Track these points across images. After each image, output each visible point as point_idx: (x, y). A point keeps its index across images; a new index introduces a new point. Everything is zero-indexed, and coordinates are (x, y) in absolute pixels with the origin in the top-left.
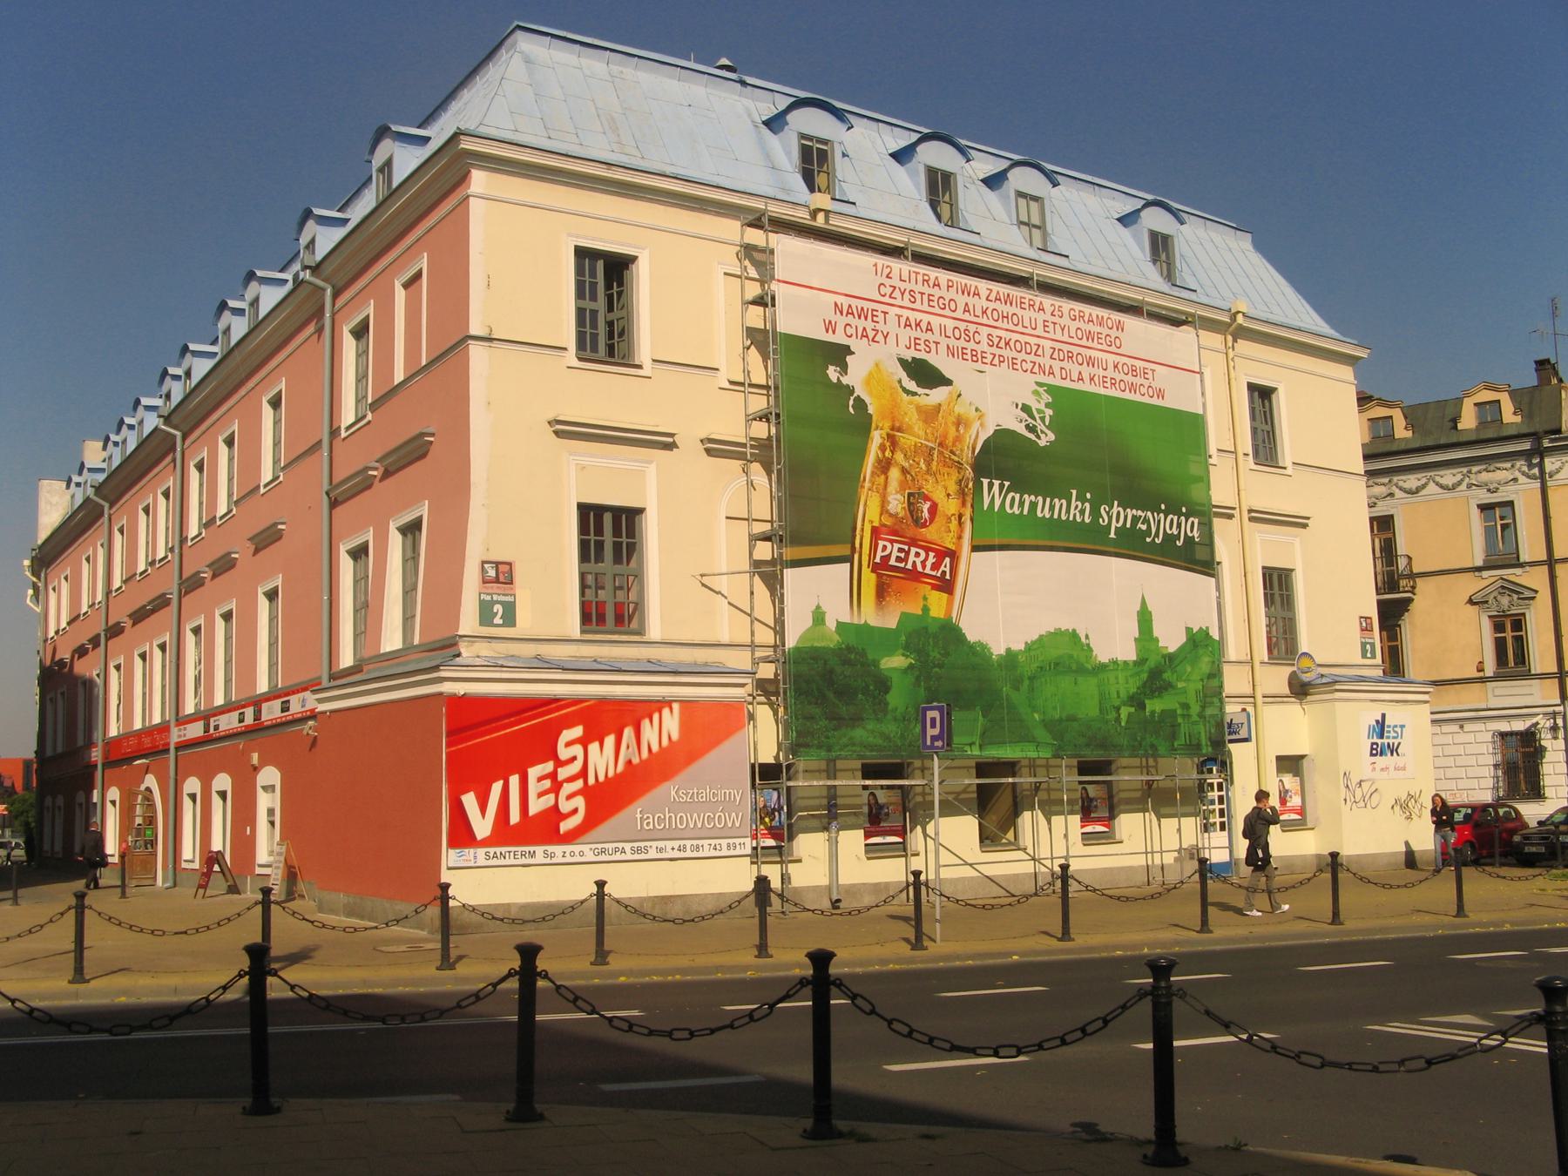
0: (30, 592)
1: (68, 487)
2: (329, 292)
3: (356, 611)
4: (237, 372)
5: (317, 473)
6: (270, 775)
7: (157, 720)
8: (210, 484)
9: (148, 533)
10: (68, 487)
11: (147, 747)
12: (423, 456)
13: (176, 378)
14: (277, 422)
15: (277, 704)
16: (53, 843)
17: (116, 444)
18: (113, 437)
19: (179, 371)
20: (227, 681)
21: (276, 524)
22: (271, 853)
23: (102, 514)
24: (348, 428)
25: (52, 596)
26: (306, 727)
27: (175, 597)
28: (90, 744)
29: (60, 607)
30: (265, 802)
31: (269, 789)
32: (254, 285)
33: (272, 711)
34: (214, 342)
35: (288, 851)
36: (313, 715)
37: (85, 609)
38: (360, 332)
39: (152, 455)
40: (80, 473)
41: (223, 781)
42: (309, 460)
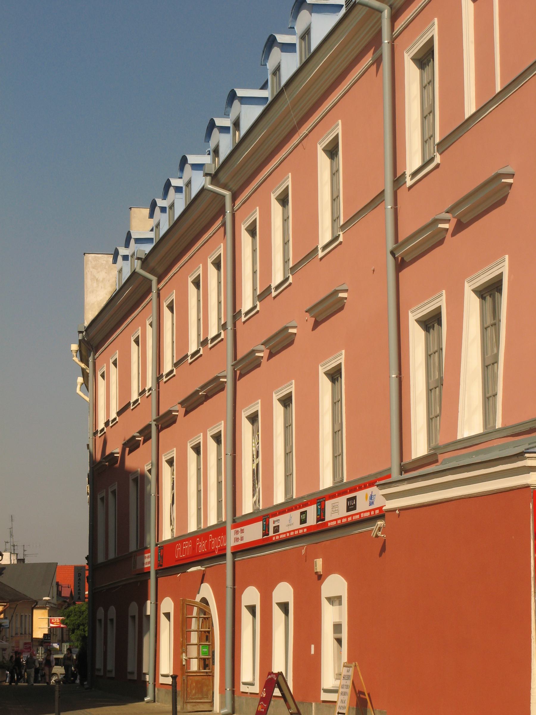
0: (80, 380)
1: (115, 261)
2: (386, 13)
3: (429, 391)
4: (289, 117)
5: (380, 229)
6: (335, 585)
7: (213, 521)
8: (264, 249)
9: (197, 309)
10: (115, 261)
11: (203, 551)
12: (502, 201)
13: (224, 130)
14: (334, 173)
15: (342, 501)
16: (105, 661)
17: (163, 210)
18: (160, 203)
19: (227, 122)
20: (288, 476)
21: (336, 292)
22: (338, 676)
23: (149, 291)
24: (414, 175)
25: (101, 383)
26: (375, 528)
27: (229, 381)
28: (143, 549)
29: (114, 392)
30: (331, 616)
31: (334, 600)
32: (304, 14)
33: (336, 510)
34: (264, 87)
35: (356, 673)
36: (381, 515)
37: (135, 396)
38: (424, 59)
39: (168, 253)
40: (127, 245)
41: (284, 592)
42: (372, 216)
